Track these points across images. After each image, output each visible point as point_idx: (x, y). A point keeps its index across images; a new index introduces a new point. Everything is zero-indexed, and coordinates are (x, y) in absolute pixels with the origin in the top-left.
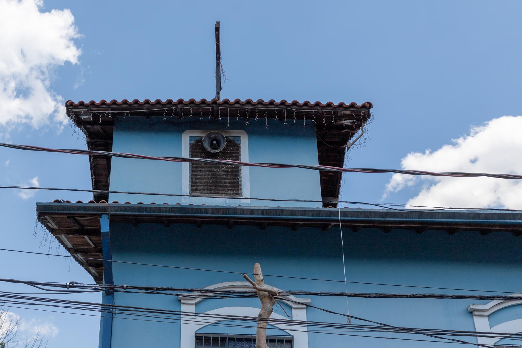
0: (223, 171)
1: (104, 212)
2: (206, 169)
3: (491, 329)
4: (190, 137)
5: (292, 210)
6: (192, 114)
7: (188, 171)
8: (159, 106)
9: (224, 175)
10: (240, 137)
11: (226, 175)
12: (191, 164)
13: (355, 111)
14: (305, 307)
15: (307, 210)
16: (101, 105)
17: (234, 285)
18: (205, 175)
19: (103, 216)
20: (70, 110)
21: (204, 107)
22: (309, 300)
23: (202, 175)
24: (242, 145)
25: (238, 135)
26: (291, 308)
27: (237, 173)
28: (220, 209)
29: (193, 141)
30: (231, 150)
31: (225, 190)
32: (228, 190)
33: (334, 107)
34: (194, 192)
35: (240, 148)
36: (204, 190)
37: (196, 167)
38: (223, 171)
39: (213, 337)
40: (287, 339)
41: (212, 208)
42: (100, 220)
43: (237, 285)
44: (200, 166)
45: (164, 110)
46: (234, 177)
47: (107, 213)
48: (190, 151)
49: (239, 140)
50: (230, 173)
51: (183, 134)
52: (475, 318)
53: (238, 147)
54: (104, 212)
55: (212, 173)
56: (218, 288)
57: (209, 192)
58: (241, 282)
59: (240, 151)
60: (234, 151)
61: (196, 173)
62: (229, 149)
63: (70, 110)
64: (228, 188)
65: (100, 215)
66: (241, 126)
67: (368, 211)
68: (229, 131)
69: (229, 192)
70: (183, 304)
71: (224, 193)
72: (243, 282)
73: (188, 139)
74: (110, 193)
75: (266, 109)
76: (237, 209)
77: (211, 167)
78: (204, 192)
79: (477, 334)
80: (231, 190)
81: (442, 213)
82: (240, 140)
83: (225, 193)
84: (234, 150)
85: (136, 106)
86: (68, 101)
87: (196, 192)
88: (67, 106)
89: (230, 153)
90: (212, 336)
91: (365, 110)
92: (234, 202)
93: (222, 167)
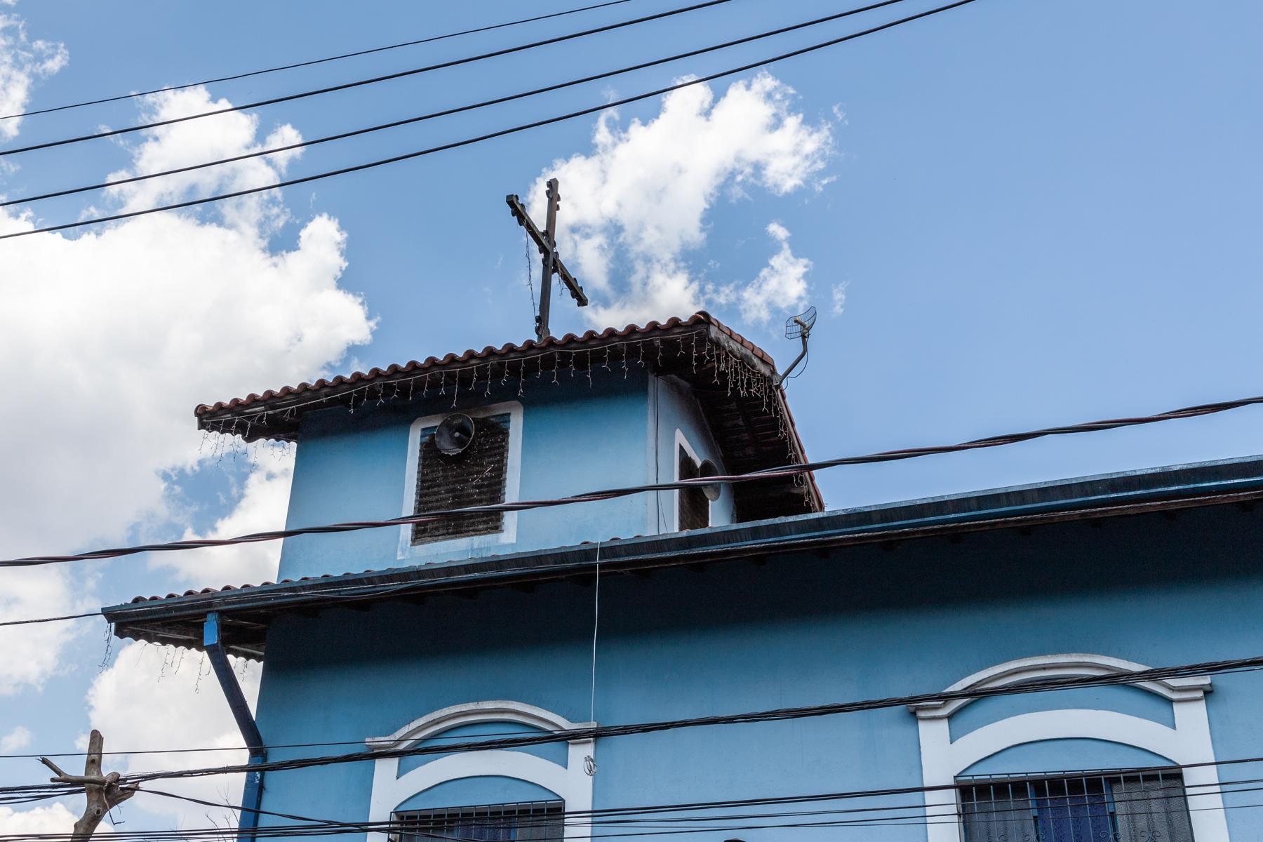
0: (474, 487)
1: (209, 609)
2: (446, 488)
3: (958, 742)
4: (423, 430)
5: (516, 559)
6: (397, 393)
7: (414, 497)
8: (345, 387)
9: (476, 493)
10: (509, 414)
11: (478, 494)
12: (420, 483)
13: (682, 333)
15: (543, 554)
16: (303, 391)
17: (463, 710)
18: (443, 499)
19: (210, 617)
20: (205, 421)
21: (417, 375)
23: (437, 501)
24: (511, 431)
25: (505, 412)
27: (498, 487)
28: (393, 575)
29: (427, 437)
30: (492, 443)
31: (473, 523)
32: (480, 523)
33: (643, 333)
34: (419, 535)
35: (508, 436)
36: (437, 529)
37: (428, 488)
38: (474, 487)
41: (379, 576)
42: (205, 623)
44: (434, 483)
45: (351, 393)
46: (492, 496)
47: (216, 609)
48: (420, 458)
49: (506, 422)
50: (486, 490)
51: (411, 429)
52: (922, 725)
53: (505, 433)
54: (209, 609)
55: (454, 494)
56: (434, 720)
57: (445, 532)
59: (507, 443)
60: (497, 445)
61: (427, 499)
62: (488, 442)
63: (205, 421)
64: (480, 519)
65: (204, 615)
66: (507, 394)
67: (654, 540)
68: (492, 406)
69: (481, 527)
71: (471, 530)
73: (419, 433)
74: (659, 480)
75: (523, 359)
76: (420, 571)
77: (454, 483)
78: (437, 533)
79: (369, 827)
80: (486, 522)
81: (794, 522)
82: (509, 421)
83: (473, 531)
84: (498, 442)
85: (308, 394)
86: (200, 405)
87: (424, 535)
88: (197, 414)
89: (490, 449)
90: (432, 814)
91: (701, 328)
92: (486, 546)
93: (473, 480)
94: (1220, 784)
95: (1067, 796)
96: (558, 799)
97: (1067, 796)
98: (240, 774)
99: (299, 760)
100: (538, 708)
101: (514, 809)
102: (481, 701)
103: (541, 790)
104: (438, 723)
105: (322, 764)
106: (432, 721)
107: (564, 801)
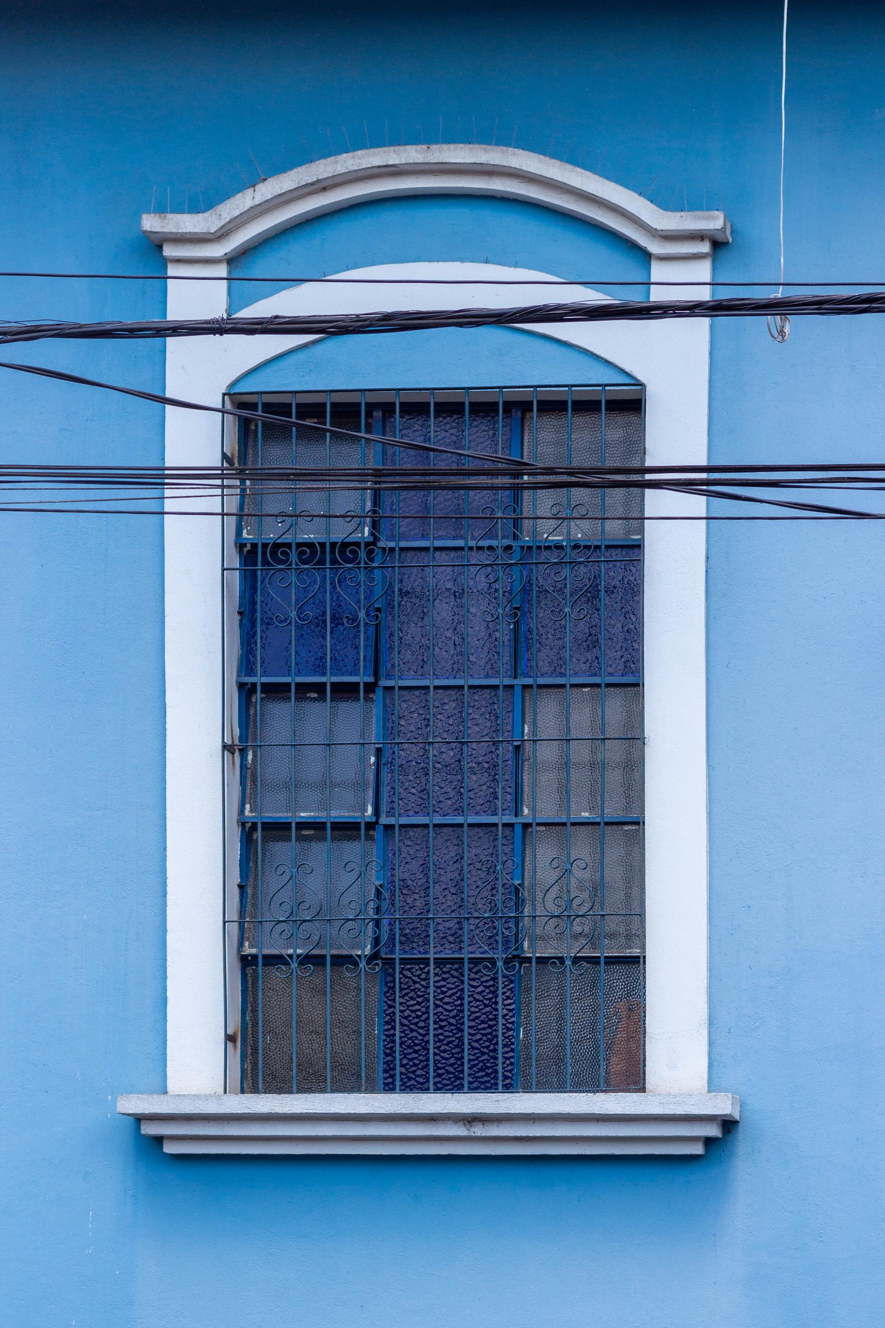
14: (705, 248)
17: (391, 162)
22: (717, 218)
26: (646, 257)
39: (298, 405)
40: (614, 398)
43: (403, 161)
56: (318, 181)
58: (425, 147)
70: (659, 262)
72: (434, 147)
90: (328, 400)
94: (262, 515)
95: (328, 566)
96: (632, 382)
97: (328, 566)
98: (170, 320)
99: (407, 313)
100: (579, 170)
101: (564, 399)
102: (437, 143)
103: (581, 358)
104: (325, 189)
105: (460, 325)
106: (312, 184)
107: (645, 387)
